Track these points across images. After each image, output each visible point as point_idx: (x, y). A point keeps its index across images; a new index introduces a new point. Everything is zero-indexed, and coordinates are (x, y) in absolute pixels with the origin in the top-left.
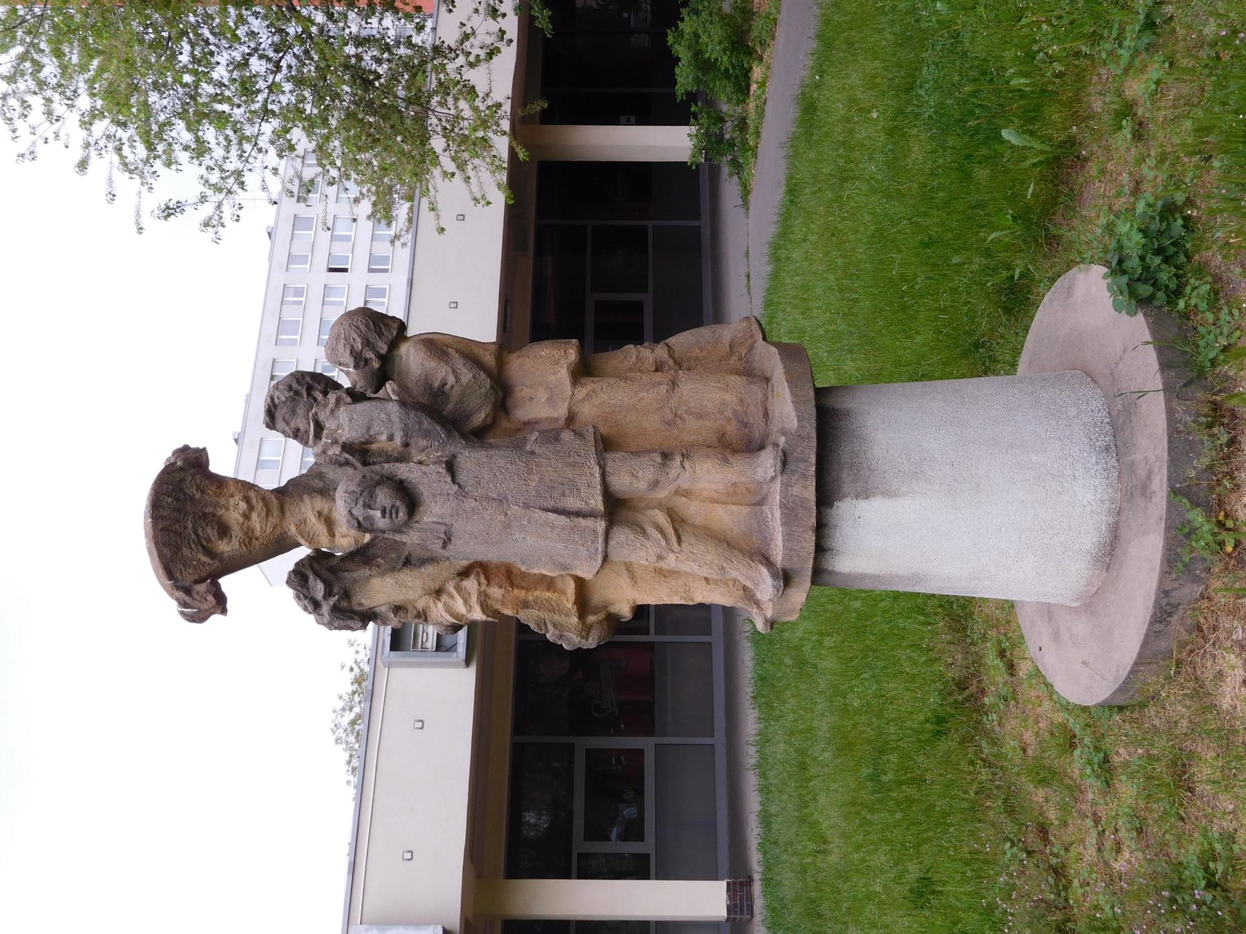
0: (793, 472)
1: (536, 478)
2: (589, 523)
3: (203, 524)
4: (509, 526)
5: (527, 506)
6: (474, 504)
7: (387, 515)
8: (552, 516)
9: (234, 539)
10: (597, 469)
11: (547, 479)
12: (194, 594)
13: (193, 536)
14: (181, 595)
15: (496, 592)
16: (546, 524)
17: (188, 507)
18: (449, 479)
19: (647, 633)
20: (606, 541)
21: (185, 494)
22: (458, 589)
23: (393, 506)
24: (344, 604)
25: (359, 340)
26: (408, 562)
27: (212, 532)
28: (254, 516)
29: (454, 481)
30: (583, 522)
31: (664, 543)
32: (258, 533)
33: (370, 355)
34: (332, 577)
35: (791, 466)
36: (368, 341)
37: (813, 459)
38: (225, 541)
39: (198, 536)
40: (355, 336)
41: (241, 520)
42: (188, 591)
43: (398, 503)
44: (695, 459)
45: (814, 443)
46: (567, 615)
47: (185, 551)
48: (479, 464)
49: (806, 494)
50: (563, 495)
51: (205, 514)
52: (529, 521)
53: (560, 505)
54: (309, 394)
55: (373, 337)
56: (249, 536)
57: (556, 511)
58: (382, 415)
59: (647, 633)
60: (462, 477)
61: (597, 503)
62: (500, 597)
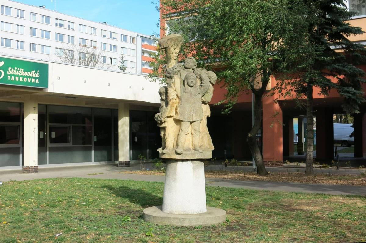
0: (200, 154)
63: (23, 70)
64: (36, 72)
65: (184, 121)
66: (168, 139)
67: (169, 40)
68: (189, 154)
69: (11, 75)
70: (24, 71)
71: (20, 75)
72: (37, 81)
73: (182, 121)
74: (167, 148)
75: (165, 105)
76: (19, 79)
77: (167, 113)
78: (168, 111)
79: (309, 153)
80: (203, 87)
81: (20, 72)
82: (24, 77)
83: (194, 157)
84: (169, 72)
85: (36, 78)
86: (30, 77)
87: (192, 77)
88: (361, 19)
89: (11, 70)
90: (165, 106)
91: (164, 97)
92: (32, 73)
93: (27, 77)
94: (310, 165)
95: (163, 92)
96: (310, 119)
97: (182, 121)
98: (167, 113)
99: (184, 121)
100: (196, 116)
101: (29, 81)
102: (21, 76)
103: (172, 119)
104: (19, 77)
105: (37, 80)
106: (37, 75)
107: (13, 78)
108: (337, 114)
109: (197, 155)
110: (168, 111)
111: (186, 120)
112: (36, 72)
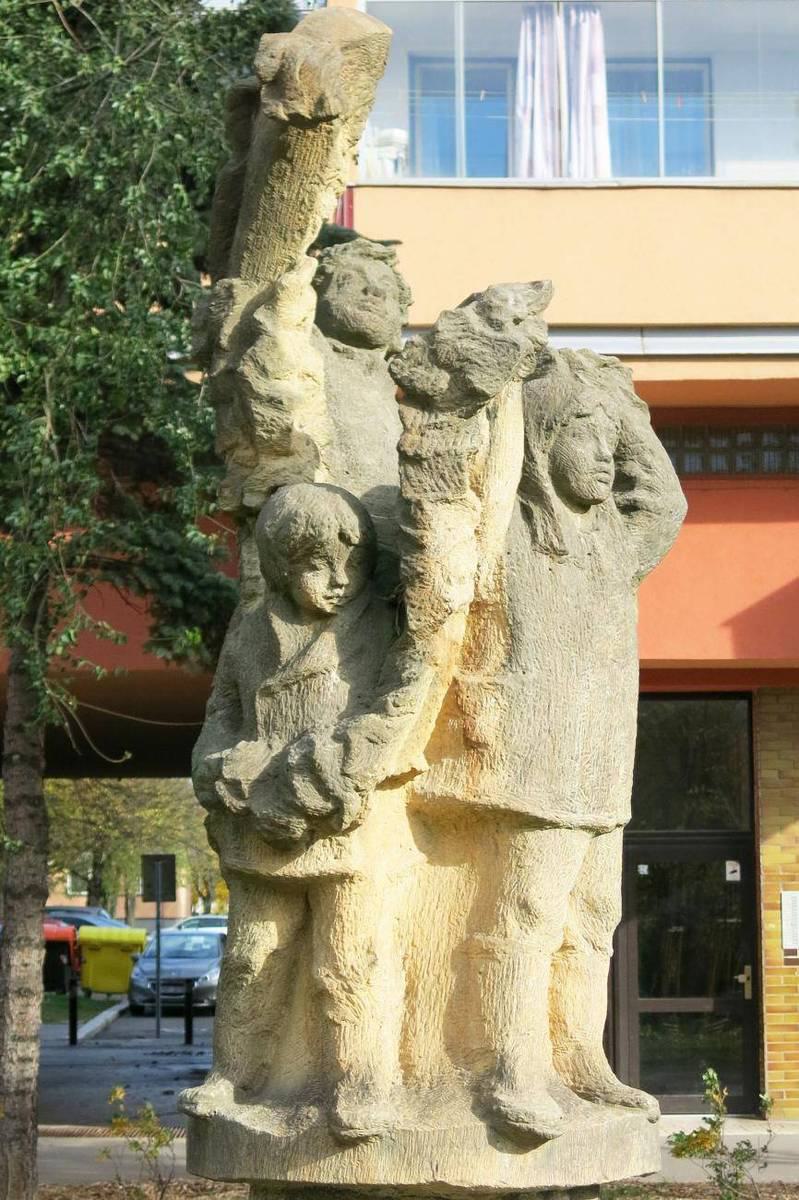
65: (555, 825)
66: (361, 994)
73: (539, 824)
74: (365, 1087)
75: (336, 660)
77: (400, 746)
79: (20, 1046)
80: (639, 517)
84: (444, 351)
87: (600, 414)
88: (745, 185)
90: (335, 676)
91: (333, 584)
94: (24, 1131)
95: (343, 536)
96: (32, 816)
97: (539, 824)
98: (400, 746)
99: (555, 825)
103: (398, 797)
108: (78, 782)
111: (578, 818)
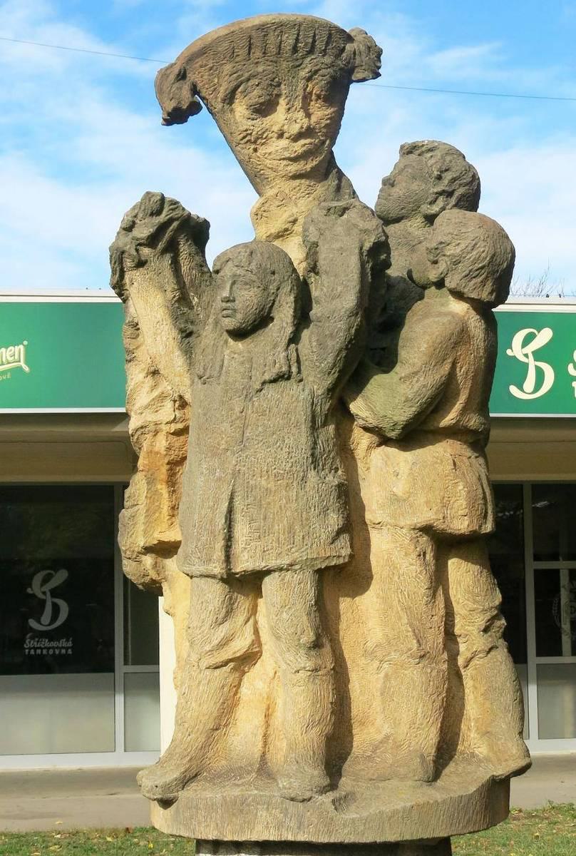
0: (285, 812)
1: (271, 485)
2: (219, 554)
3: (265, 83)
4: (214, 455)
5: (236, 474)
6: (237, 410)
7: (224, 305)
8: (224, 506)
9: (250, 122)
10: (285, 561)
11: (270, 499)
12: (177, 85)
13: (246, 75)
14: (176, 70)
15: (161, 443)
16: (217, 501)
17: (284, 65)
18: (267, 377)
19: (539, 654)
20: (202, 576)
21: (303, 58)
22: (162, 397)
23: (235, 310)
24: (128, 263)
25: (458, 250)
26: (187, 334)
27: (256, 95)
28: (284, 143)
29: (264, 383)
30: (220, 544)
31: (208, 648)
32: (262, 150)
33: (442, 266)
34: (161, 246)
35: (292, 808)
36: (457, 263)
37: (302, 838)
38: (247, 113)
39: (248, 80)
40: (463, 246)
41: (276, 128)
42: (182, 76)
43: (239, 316)
44: (311, 686)
45: (324, 839)
46: (145, 532)
47: (228, 68)
48: (288, 412)
49: (259, 828)
50: (252, 520)
51: (279, 85)
52: (219, 479)
53: (238, 516)
54: (440, 194)
55: (463, 268)
56: (257, 140)
57: (230, 511)
58: (339, 289)
59: (539, 654)
60: (271, 391)
61: (245, 563)
62: (156, 449)
63: (47, 640)
64: (67, 641)
67: (200, 61)
68: (211, 807)
69: (30, 649)
70: (49, 641)
71: (43, 646)
72: (70, 652)
76: (42, 652)
78: (142, 508)
81: (43, 643)
82: (48, 649)
83: (242, 830)
85: (67, 649)
86: (57, 648)
89: (30, 642)
92: (61, 642)
93: (53, 648)
100: (260, 534)
101: (57, 652)
102: (45, 648)
104: (42, 649)
105: (70, 650)
106: (70, 644)
107: (32, 652)
109: (262, 814)
110: (142, 508)
112: (67, 641)
